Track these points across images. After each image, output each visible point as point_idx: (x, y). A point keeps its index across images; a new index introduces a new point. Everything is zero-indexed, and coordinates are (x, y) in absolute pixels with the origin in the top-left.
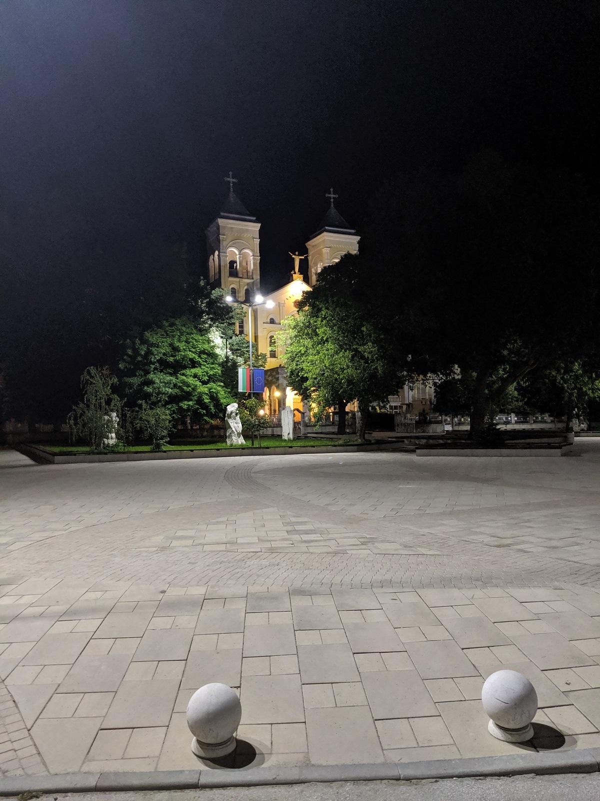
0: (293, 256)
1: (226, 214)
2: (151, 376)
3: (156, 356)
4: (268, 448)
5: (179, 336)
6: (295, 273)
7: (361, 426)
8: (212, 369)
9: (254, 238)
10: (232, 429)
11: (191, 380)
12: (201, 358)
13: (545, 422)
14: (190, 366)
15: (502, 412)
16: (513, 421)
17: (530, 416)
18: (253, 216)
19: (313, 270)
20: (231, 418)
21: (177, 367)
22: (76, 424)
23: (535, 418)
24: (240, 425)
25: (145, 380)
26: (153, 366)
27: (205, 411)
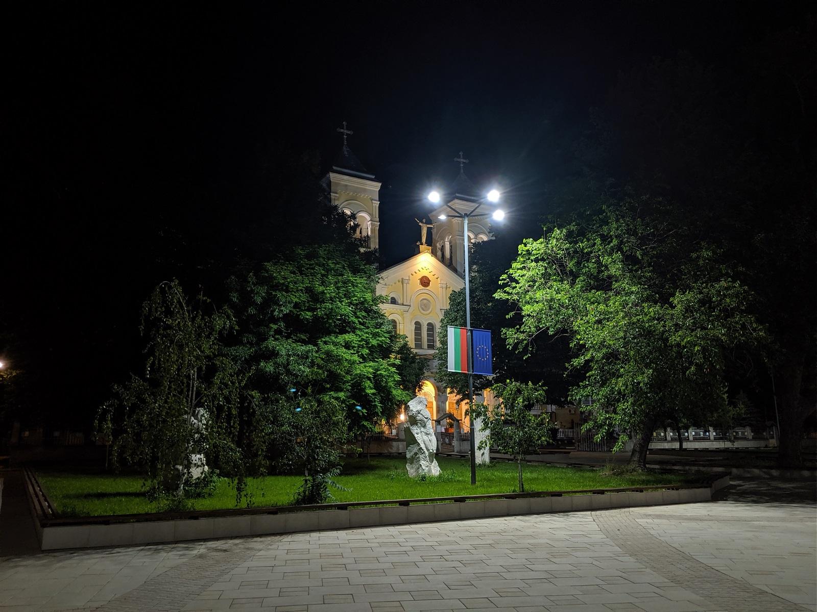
0: (420, 224)
1: (339, 169)
2: (271, 343)
3: (283, 308)
4: (559, 494)
5: (323, 275)
6: (422, 244)
7: (640, 444)
8: (375, 335)
9: (372, 200)
10: (419, 444)
11: (342, 352)
12: (357, 317)
13: (745, 439)
14: (337, 330)
15: (697, 425)
16: (712, 438)
17: (730, 431)
18: (372, 174)
19: (438, 245)
20: (417, 424)
21: (316, 330)
22: (117, 433)
23: (735, 434)
24: (434, 438)
25: (256, 351)
26: (275, 327)
27: (365, 411)
